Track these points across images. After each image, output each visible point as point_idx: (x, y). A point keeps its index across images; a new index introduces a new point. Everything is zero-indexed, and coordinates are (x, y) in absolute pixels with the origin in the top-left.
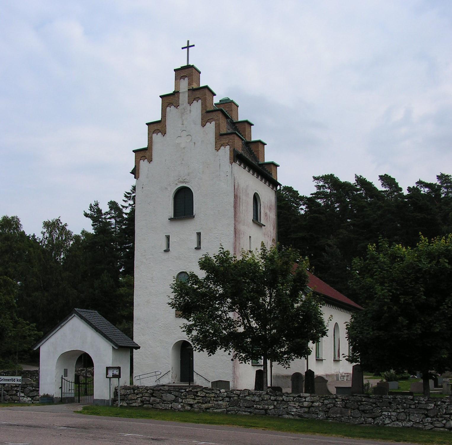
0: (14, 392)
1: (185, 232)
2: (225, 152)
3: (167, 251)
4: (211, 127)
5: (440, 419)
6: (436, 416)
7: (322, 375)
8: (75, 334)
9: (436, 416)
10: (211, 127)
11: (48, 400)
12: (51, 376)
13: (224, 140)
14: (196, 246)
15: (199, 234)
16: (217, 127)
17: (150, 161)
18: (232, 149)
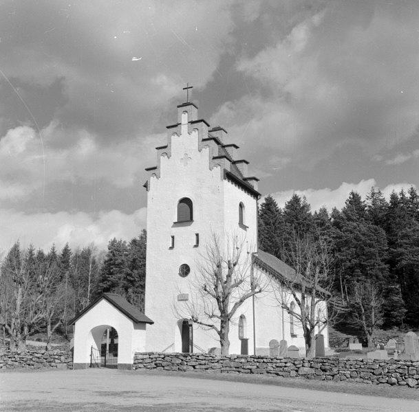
0: (52, 359)
1: (185, 234)
2: (218, 171)
3: (196, 246)
4: (206, 151)
5: (384, 376)
6: (381, 374)
7: (73, 342)
8: (104, 314)
9: (381, 374)
10: (206, 151)
11: (81, 366)
12: (84, 345)
13: (217, 161)
14: (195, 244)
15: (197, 235)
16: (211, 151)
17: (158, 177)
18: (223, 169)
